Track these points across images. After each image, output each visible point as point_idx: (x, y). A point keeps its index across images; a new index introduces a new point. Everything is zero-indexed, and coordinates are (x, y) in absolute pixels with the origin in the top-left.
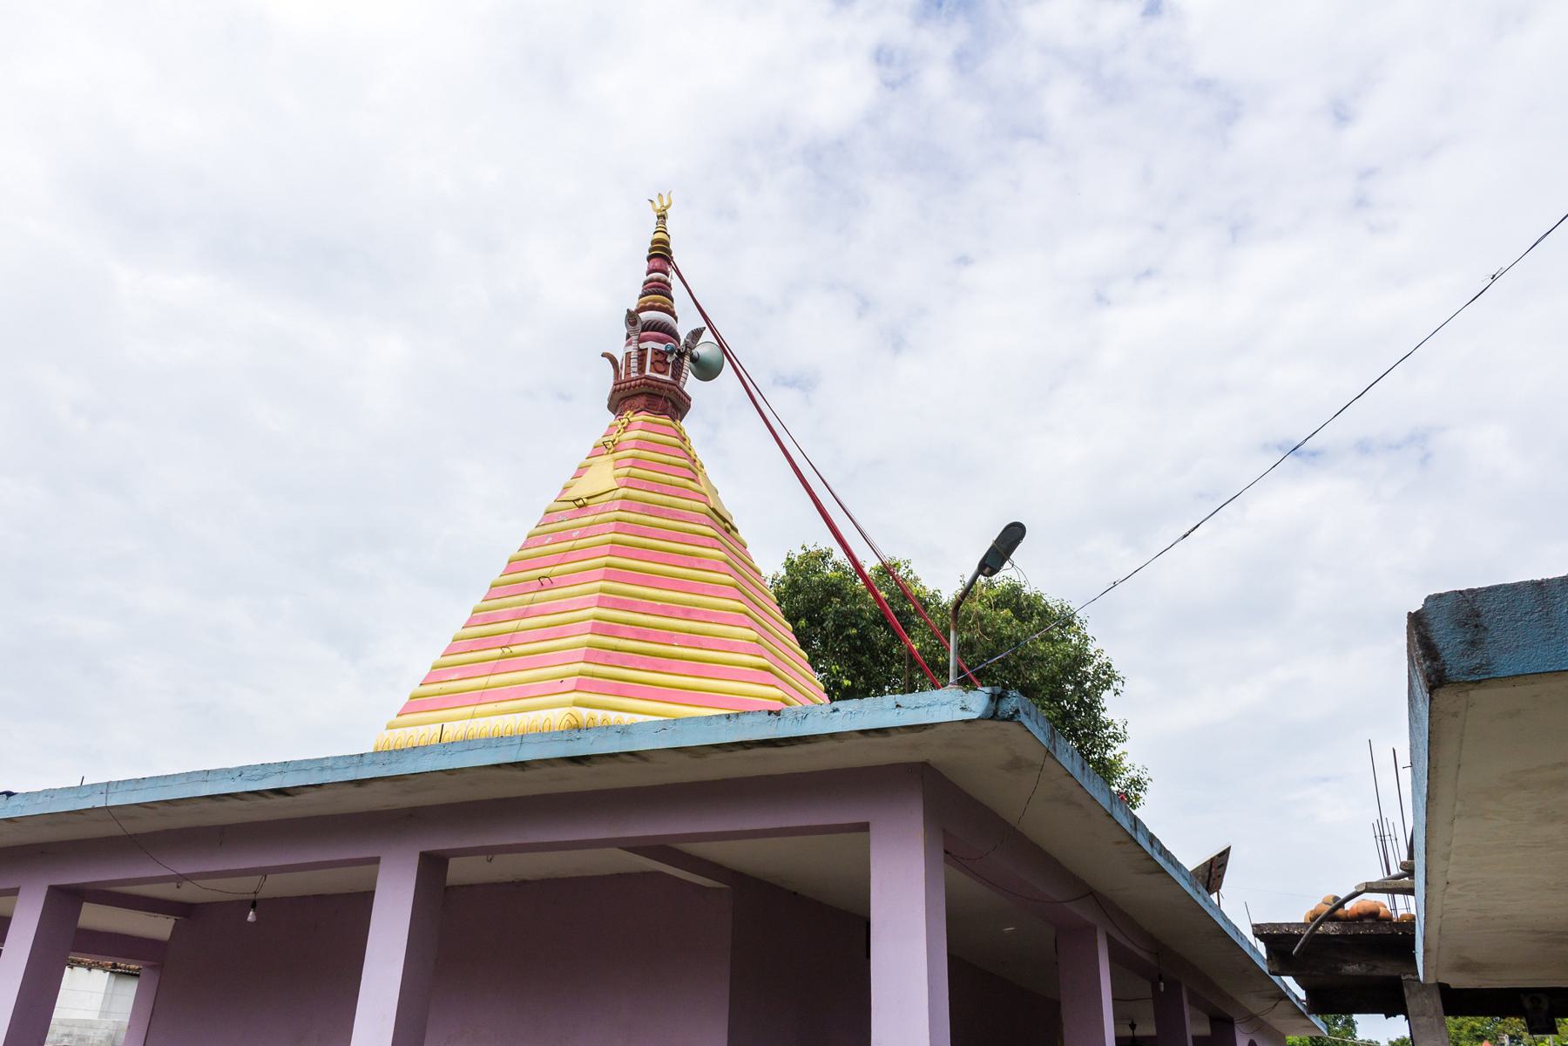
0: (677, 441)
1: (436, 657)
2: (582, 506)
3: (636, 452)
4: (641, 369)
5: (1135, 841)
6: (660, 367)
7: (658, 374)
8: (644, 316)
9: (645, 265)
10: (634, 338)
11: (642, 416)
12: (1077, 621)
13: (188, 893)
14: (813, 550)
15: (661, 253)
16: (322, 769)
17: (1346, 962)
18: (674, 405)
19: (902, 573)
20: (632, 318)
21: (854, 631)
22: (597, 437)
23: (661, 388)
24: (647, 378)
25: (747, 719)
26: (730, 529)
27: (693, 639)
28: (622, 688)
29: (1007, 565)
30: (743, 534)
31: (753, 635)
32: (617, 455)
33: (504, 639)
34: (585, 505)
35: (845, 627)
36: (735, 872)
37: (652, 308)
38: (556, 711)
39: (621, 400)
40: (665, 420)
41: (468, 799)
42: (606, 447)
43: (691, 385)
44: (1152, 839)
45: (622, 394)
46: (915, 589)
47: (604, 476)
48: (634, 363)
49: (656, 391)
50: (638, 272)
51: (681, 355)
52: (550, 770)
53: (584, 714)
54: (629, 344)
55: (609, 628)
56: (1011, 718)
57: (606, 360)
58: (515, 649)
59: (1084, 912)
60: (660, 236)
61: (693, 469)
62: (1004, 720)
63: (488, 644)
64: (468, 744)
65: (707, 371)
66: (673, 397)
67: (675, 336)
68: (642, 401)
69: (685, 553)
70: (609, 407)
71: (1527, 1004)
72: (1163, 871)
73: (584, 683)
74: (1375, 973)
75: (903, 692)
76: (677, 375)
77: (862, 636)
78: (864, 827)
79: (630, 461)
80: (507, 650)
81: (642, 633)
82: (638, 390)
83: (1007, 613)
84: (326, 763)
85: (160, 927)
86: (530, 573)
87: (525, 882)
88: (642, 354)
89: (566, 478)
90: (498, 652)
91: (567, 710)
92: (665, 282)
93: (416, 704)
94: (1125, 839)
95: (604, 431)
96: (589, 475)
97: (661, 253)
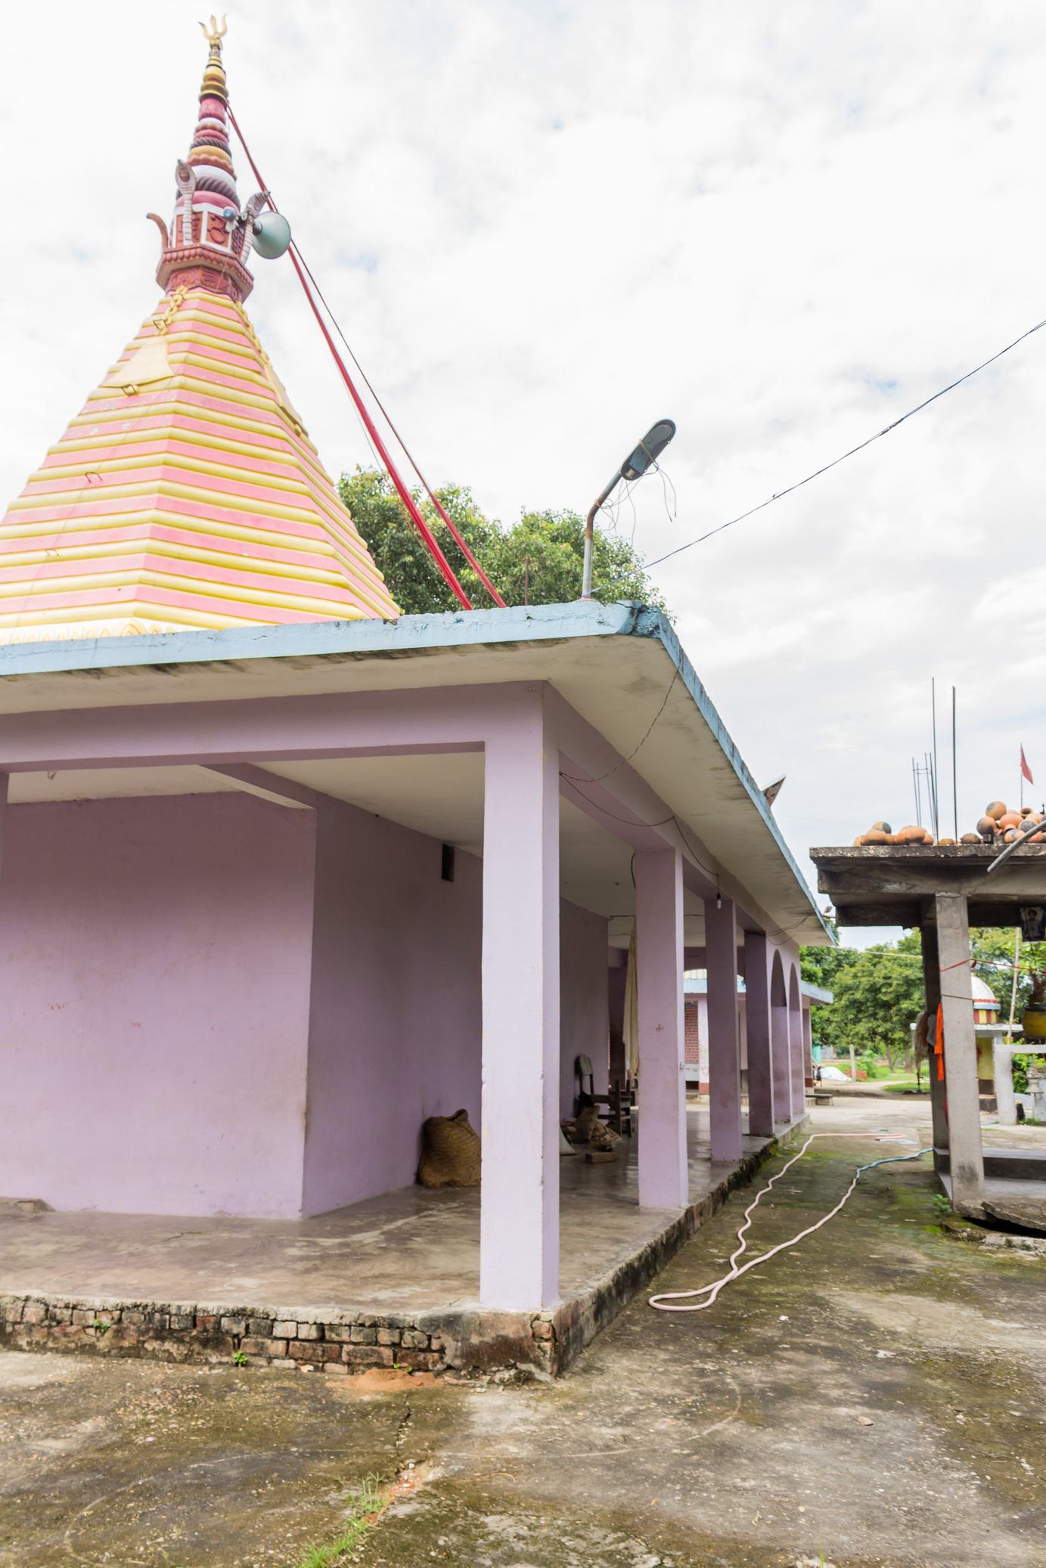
2: (131, 393)
4: (196, 237)
5: (732, 767)
6: (219, 237)
7: (216, 249)
8: (200, 171)
10: (186, 197)
11: (199, 293)
14: (369, 471)
15: (215, 94)
17: (888, 881)
18: (235, 285)
19: (461, 501)
20: (184, 172)
21: (409, 559)
23: (219, 262)
24: (203, 248)
26: (300, 433)
27: (265, 550)
28: (188, 599)
29: (651, 468)
30: (313, 439)
31: (329, 548)
32: (171, 337)
34: (135, 393)
35: (401, 554)
36: (320, 794)
37: (206, 162)
38: (116, 622)
39: (175, 270)
40: (225, 300)
42: (158, 327)
43: (253, 261)
44: (743, 766)
45: (173, 266)
46: (474, 520)
47: (155, 361)
48: (187, 228)
49: (214, 265)
51: (242, 223)
52: (127, 678)
54: (181, 204)
55: (171, 534)
56: (650, 634)
57: (153, 224)
58: (62, 552)
59: (666, 836)
60: (213, 70)
61: (258, 361)
62: (643, 636)
64: (33, 648)
65: (271, 247)
68: (197, 276)
70: (158, 280)
71: (1024, 916)
72: (748, 798)
73: (146, 592)
74: (913, 891)
75: (534, 604)
76: (237, 248)
77: (419, 564)
78: (480, 747)
80: (52, 553)
81: (208, 540)
82: (192, 262)
83: (567, 547)
87: (88, 801)
88: (197, 218)
90: (43, 555)
91: (128, 621)
92: (221, 131)
94: (721, 763)
97: (215, 94)
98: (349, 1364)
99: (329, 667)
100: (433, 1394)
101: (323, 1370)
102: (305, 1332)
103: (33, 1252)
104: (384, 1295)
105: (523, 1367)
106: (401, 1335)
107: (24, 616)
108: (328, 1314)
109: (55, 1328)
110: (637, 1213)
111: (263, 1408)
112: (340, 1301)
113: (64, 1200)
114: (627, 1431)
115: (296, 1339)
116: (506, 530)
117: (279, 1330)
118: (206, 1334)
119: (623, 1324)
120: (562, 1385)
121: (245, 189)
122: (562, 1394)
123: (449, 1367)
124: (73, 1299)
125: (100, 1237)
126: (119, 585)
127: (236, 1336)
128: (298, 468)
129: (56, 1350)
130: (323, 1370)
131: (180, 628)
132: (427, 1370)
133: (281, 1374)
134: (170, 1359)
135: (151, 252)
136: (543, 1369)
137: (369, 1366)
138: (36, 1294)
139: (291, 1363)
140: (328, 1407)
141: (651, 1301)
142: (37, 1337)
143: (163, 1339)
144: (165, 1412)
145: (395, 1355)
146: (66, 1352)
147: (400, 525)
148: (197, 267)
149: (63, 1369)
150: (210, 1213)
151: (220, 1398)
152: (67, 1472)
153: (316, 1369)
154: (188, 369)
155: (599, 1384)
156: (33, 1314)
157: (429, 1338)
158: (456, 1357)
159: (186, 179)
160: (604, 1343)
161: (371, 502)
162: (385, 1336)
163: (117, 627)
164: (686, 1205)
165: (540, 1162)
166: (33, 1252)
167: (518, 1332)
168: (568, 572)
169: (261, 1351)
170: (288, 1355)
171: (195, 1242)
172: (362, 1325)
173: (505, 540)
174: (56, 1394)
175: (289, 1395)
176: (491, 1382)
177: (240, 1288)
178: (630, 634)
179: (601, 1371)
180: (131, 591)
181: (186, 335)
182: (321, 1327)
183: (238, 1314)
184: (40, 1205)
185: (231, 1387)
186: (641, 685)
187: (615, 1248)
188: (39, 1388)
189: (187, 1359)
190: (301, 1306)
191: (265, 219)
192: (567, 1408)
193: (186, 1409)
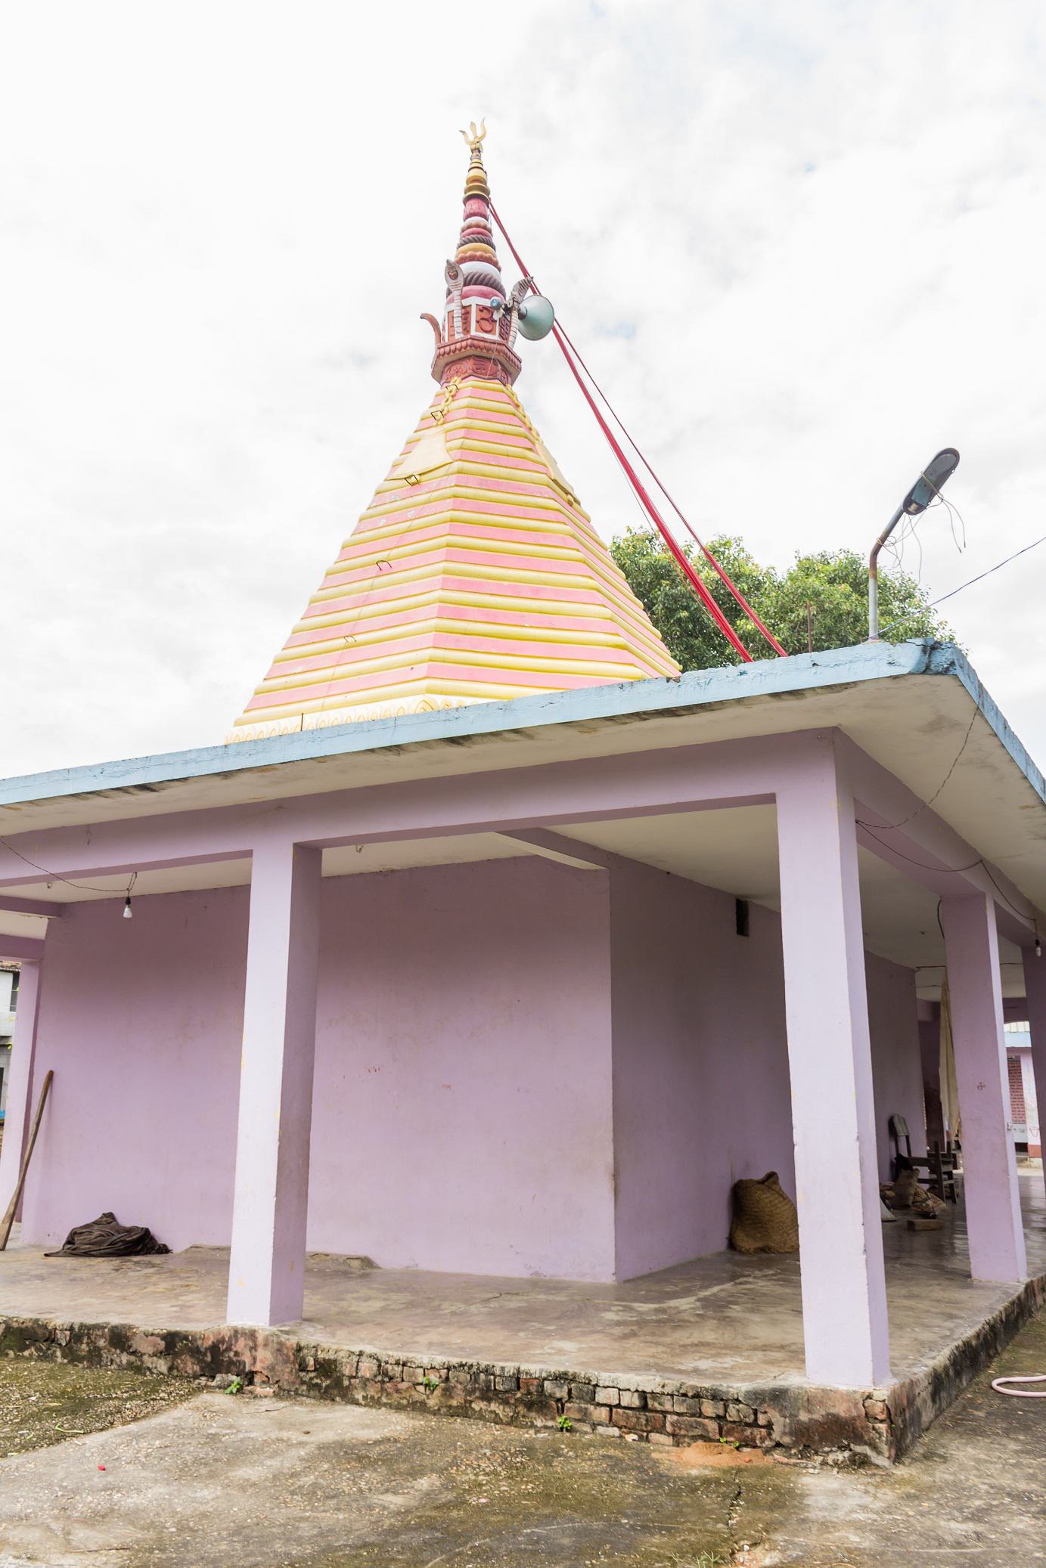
0: (511, 408)
1: (277, 650)
2: (413, 482)
3: (467, 422)
6: (487, 326)
7: (486, 337)
8: (467, 268)
9: (460, 209)
10: (456, 294)
11: (472, 381)
12: (917, 594)
13: (60, 892)
14: (639, 532)
15: (478, 194)
16: (186, 762)
18: (504, 369)
20: (452, 271)
21: (684, 614)
22: (424, 406)
25: (642, 688)
26: (573, 502)
28: (476, 673)
29: (936, 500)
30: (585, 507)
31: (607, 612)
33: (346, 629)
34: (418, 482)
35: (676, 610)
37: (473, 258)
38: (410, 699)
39: (447, 364)
40: (496, 385)
41: (343, 787)
42: (437, 417)
43: (520, 345)
45: (447, 359)
46: (747, 569)
47: (434, 451)
48: (458, 323)
49: (484, 353)
50: (454, 217)
51: (508, 310)
53: (439, 701)
54: (451, 301)
59: (975, 880)
60: (475, 173)
61: (529, 438)
62: (938, 673)
63: (331, 628)
65: (536, 329)
66: (503, 360)
67: (498, 287)
68: (468, 365)
69: (529, 529)
73: (437, 669)
76: (504, 335)
77: (695, 619)
78: (771, 799)
79: (462, 432)
80: (350, 639)
81: (491, 615)
83: (846, 588)
84: (189, 757)
85: (35, 926)
86: (368, 556)
87: (392, 871)
88: (466, 312)
89: (395, 455)
90: (343, 641)
91: (420, 697)
92: (485, 227)
93: (263, 698)
95: (430, 401)
96: (419, 450)
97: (478, 194)
98: (674, 1435)
99: (614, 728)
100: (763, 1473)
101: (647, 1440)
102: (627, 1399)
103: (364, 1308)
104: (704, 1364)
105: (858, 1449)
106: (726, 1407)
107: (329, 701)
108: (650, 1382)
109: (388, 1384)
110: (970, 1286)
111: (591, 1476)
112: (661, 1369)
113: (389, 1259)
114: (980, 1528)
115: (619, 1406)
116: (781, 576)
117: (601, 1396)
118: (530, 1397)
119: (964, 1408)
120: (901, 1471)
121: (509, 278)
122: (902, 1482)
123: (778, 1445)
124: (402, 1356)
125: (424, 1295)
126: (411, 665)
127: (559, 1400)
128: (573, 536)
129: (389, 1406)
130: (647, 1440)
131: (469, 701)
132: (755, 1447)
133: (606, 1442)
134: (497, 1420)
135: (424, 347)
136: (879, 1453)
137: (694, 1438)
138: (369, 1349)
139: (616, 1431)
140: (657, 1479)
141: (994, 1383)
142: (372, 1392)
143: (489, 1400)
144: (495, 1473)
145: (721, 1429)
146: (399, 1408)
147: (673, 581)
148: (468, 357)
149: (397, 1425)
150: (526, 1275)
151: (548, 1463)
152: (408, 1528)
153: (641, 1438)
154: (465, 454)
155: (942, 1474)
156: (367, 1369)
157: (755, 1412)
158: (784, 1433)
159: (455, 277)
160: (944, 1428)
161: (643, 562)
162: (709, 1408)
163: (411, 704)
164: (1025, 1279)
165: (861, 1229)
166: (364, 1308)
167: (849, 1410)
168: (848, 613)
169: (585, 1417)
170: (611, 1422)
171: (513, 1304)
172: (685, 1395)
173: (780, 587)
174: (393, 1449)
175: (616, 1464)
176: (824, 1463)
177: (560, 1352)
178: (924, 673)
179: (944, 1459)
180: (422, 669)
181: (462, 422)
182: (643, 1395)
183: (560, 1378)
184: (367, 1262)
185: (557, 1453)
186: (937, 725)
187: (949, 1324)
188: (376, 1443)
189: (513, 1421)
190: (624, 1377)
191: (530, 304)
192: (909, 1496)
193: (515, 1472)
